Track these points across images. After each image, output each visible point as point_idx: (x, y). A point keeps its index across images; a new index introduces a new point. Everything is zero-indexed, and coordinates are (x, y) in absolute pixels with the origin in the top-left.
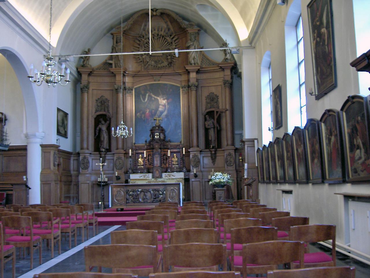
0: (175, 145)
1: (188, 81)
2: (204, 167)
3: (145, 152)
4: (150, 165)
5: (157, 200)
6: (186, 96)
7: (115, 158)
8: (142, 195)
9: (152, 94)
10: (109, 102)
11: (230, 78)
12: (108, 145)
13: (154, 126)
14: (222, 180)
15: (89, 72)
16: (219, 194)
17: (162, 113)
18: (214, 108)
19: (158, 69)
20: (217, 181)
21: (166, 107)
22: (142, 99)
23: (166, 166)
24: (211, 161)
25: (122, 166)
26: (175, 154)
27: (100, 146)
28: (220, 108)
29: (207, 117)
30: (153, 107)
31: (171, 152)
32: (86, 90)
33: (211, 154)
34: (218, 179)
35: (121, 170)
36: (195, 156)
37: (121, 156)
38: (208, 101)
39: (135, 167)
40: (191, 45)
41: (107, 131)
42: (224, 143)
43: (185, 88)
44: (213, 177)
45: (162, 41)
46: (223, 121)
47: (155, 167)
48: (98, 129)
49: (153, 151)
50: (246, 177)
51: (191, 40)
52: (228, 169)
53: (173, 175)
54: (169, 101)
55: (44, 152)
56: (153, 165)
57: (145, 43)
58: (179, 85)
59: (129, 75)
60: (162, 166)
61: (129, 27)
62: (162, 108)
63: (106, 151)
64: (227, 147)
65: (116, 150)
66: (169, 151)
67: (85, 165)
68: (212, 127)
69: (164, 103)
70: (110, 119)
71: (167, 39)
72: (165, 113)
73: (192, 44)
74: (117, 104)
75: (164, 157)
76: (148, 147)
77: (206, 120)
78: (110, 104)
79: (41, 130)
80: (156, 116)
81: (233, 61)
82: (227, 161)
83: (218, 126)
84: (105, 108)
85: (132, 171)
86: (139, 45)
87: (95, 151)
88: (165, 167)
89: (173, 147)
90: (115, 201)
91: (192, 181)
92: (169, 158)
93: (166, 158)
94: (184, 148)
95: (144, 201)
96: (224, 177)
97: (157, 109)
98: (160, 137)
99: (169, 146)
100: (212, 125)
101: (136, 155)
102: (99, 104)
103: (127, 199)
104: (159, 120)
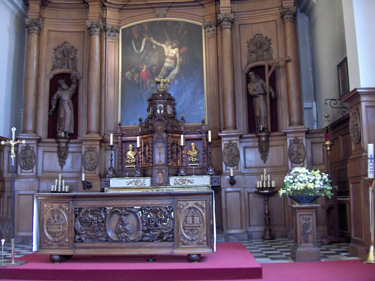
0: (193, 127)
2: (247, 166)
3: (138, 138)
4: (148, 162)
5: (153, 236)
6: (212, 41)
7: (83, 150)
9: (152, 38)
10: (77, 52)
12: (72, 126)
13: (156, 92)
14: (311, 186)
16: (303, 218)
17: (169, 70)
18: (263, 60)
20: (300, 186)
22: (134, 47)
23: (177, 164)
24: (259, 155)
25: (96, 164)
26: (193, 144)
28: (275, 56)
29: (251, 75)
30: (154, 60)
31: (186, 140)
32: (35, 30)
33: (259, 141)
34: (301, 182)
35: (94, 171)
36: (230, 145)
37: (94, 146)
38: (252, 48)
39: (120, 166)
41: (71, 102)
44: (287, 178)
46: (281, 83)
47: (157, 165)
49: (153, 137)
56: (153, 163)
58: (201, 24)
62: (170, 63)
63: (68, 137)
64: (291, 128)
65: (86, 135)
66: (182, 136)
67: (27, 161)
68: (262, 92)
69: (173, 54)
72: (175, 71)
74: (89, 55)
75: (174, 147)
76: (143, 129)
77: (248, 80)
78: (77, 56)
80: (160, 76)
82: (293, 154)
83: (271, 90)
84: (68, 61)
85: (114, 172)
87: (49, 136)
88: (175, 165)
89: (189, 131)
90: (47, 234)
91: (226, 192)
92: (182, 150)
93: (177, 149)
94: (210, 132)
95: (118, 237)
96: (314, 178)
98: (165, 111)
99: (183, 128)
100: (261, 89)
101: (122, 145)
103: (75, 230)
104: (164, 83)
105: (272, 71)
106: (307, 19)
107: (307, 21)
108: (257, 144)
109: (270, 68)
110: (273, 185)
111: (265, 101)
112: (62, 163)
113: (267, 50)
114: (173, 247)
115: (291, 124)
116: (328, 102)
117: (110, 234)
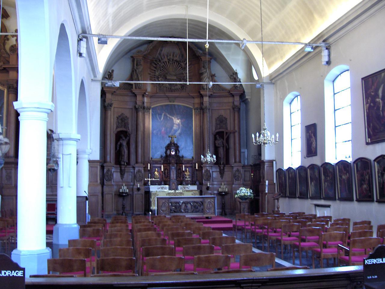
1: (202, 103)
6: (198, 117)
8: (183, 206)
9: (167, 114)
11: (239, 103)
12: (127, 159)
14: (246, 194)
15: (113, 92)
17: (176, 131)
19: (172, 91)
20: (243, 194)
21: (180, 126)
24: (219, 175)
25: (142, 179)
27: (120, 159)
28: (229, 129)
40: (204, 72)
41: (127, 146)
42: (232, 160)
43: (197, 109)
44: (238, 191)
45: (176, 66)
48: (119, 143)
50: (267, 192)
51: (204, 67)
53: (187, 188)
55: (91, 167)
56: (170, 179)
57: (161, 66)
58: (192, 107)
59: (147, 96)
60: (178, 179)
61: (149, 52)
62: (176, 127)
64: (235, 164)
69: (178, 122)
70: (130, 135)
71: (181, 64)
73: (205, 71)
77: (215, 139)
79: (89, 147)
81: (242, 89)
82: (236, 176)
83: (227, 145)
86: (155, 68)
97: (172, 128)
100: (221, 143)
102: (120, 121)
105: (227, 136)
106: (244, 105)
107: (245, 107)
108: (218, 170)
110: (227, 191)
111: (223, 150)
113: (225, 124)
114: (203, 214)
115: (235, 162)
116: (253, 157)
117: (182, 211)
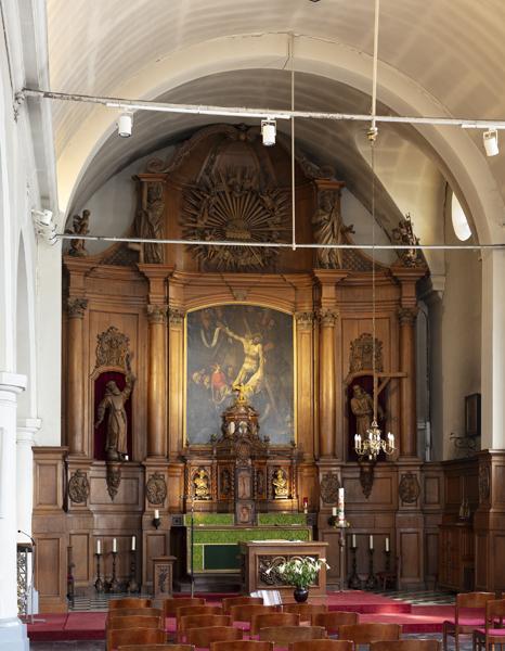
19: (239, 272)
22: (204, 339)
27: (107, 446)
41: (123, 411)
46: (392, 401)
51: (323, 208)
52: (405, 508)
54: (266, 348)
55: (40, 465)
82: (404, 491)
86: (198, 209)
102: (106, 348)
105: (382, 387)
109: (380, 383)
112: (112, 492)
